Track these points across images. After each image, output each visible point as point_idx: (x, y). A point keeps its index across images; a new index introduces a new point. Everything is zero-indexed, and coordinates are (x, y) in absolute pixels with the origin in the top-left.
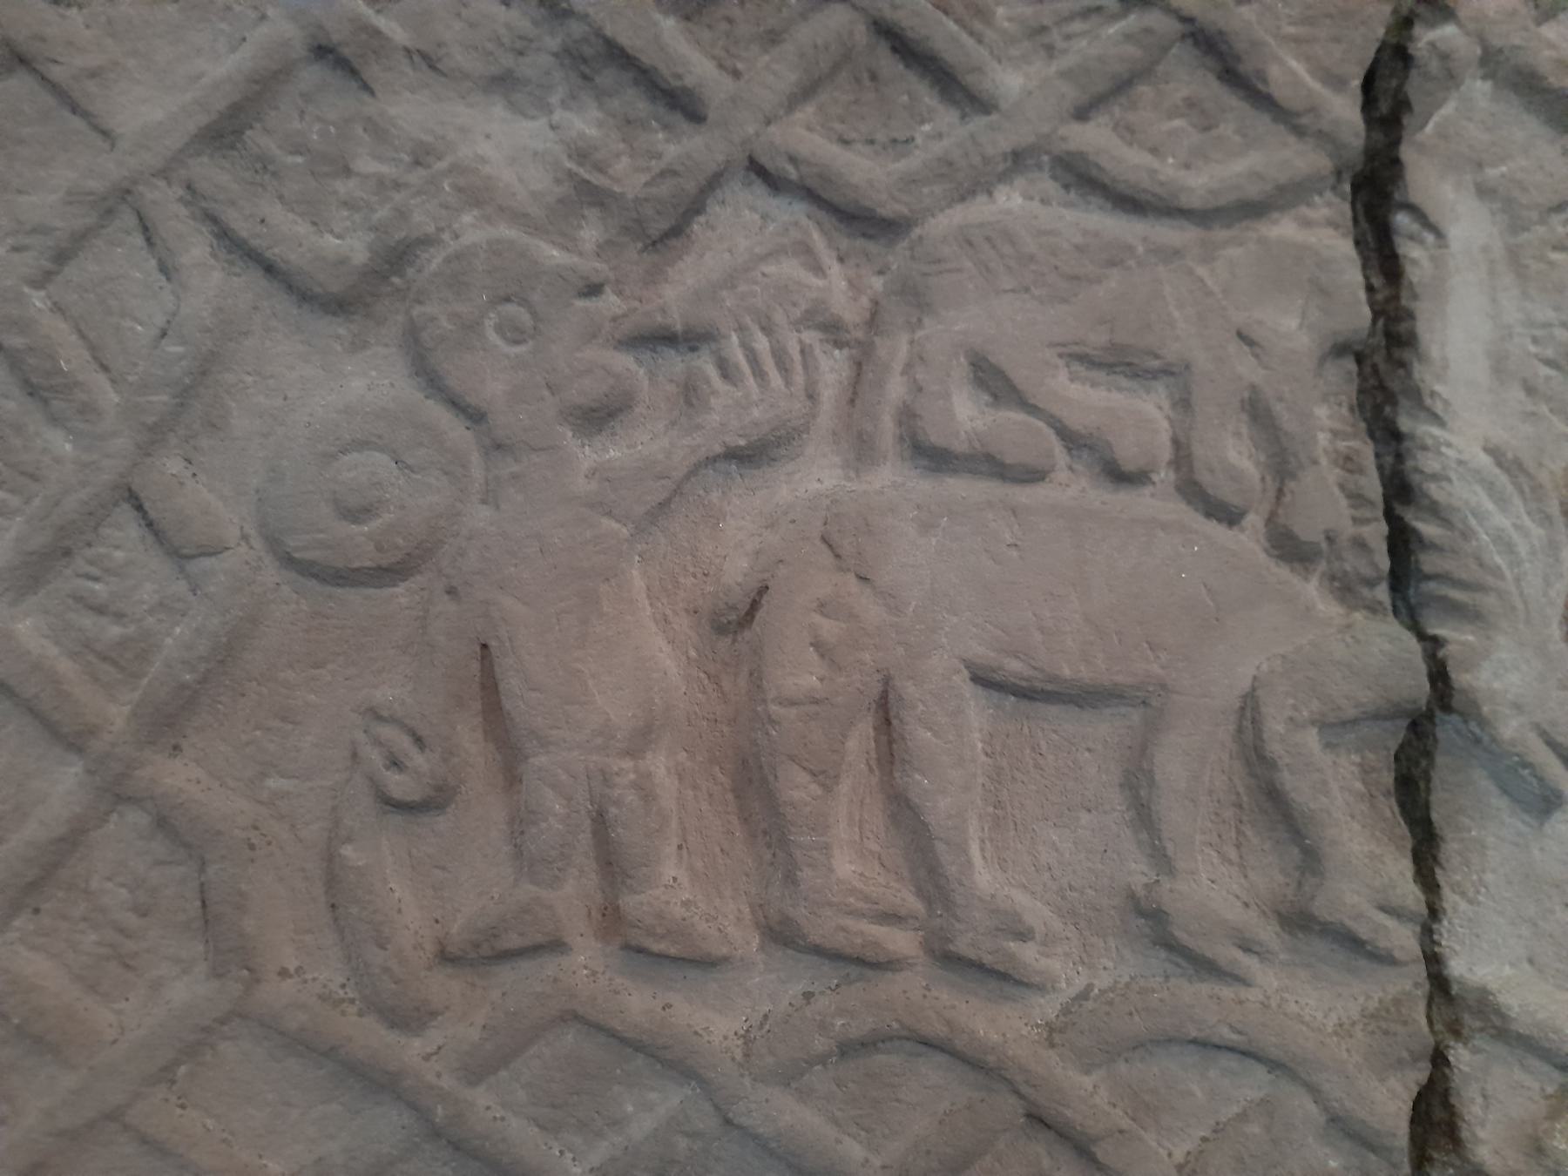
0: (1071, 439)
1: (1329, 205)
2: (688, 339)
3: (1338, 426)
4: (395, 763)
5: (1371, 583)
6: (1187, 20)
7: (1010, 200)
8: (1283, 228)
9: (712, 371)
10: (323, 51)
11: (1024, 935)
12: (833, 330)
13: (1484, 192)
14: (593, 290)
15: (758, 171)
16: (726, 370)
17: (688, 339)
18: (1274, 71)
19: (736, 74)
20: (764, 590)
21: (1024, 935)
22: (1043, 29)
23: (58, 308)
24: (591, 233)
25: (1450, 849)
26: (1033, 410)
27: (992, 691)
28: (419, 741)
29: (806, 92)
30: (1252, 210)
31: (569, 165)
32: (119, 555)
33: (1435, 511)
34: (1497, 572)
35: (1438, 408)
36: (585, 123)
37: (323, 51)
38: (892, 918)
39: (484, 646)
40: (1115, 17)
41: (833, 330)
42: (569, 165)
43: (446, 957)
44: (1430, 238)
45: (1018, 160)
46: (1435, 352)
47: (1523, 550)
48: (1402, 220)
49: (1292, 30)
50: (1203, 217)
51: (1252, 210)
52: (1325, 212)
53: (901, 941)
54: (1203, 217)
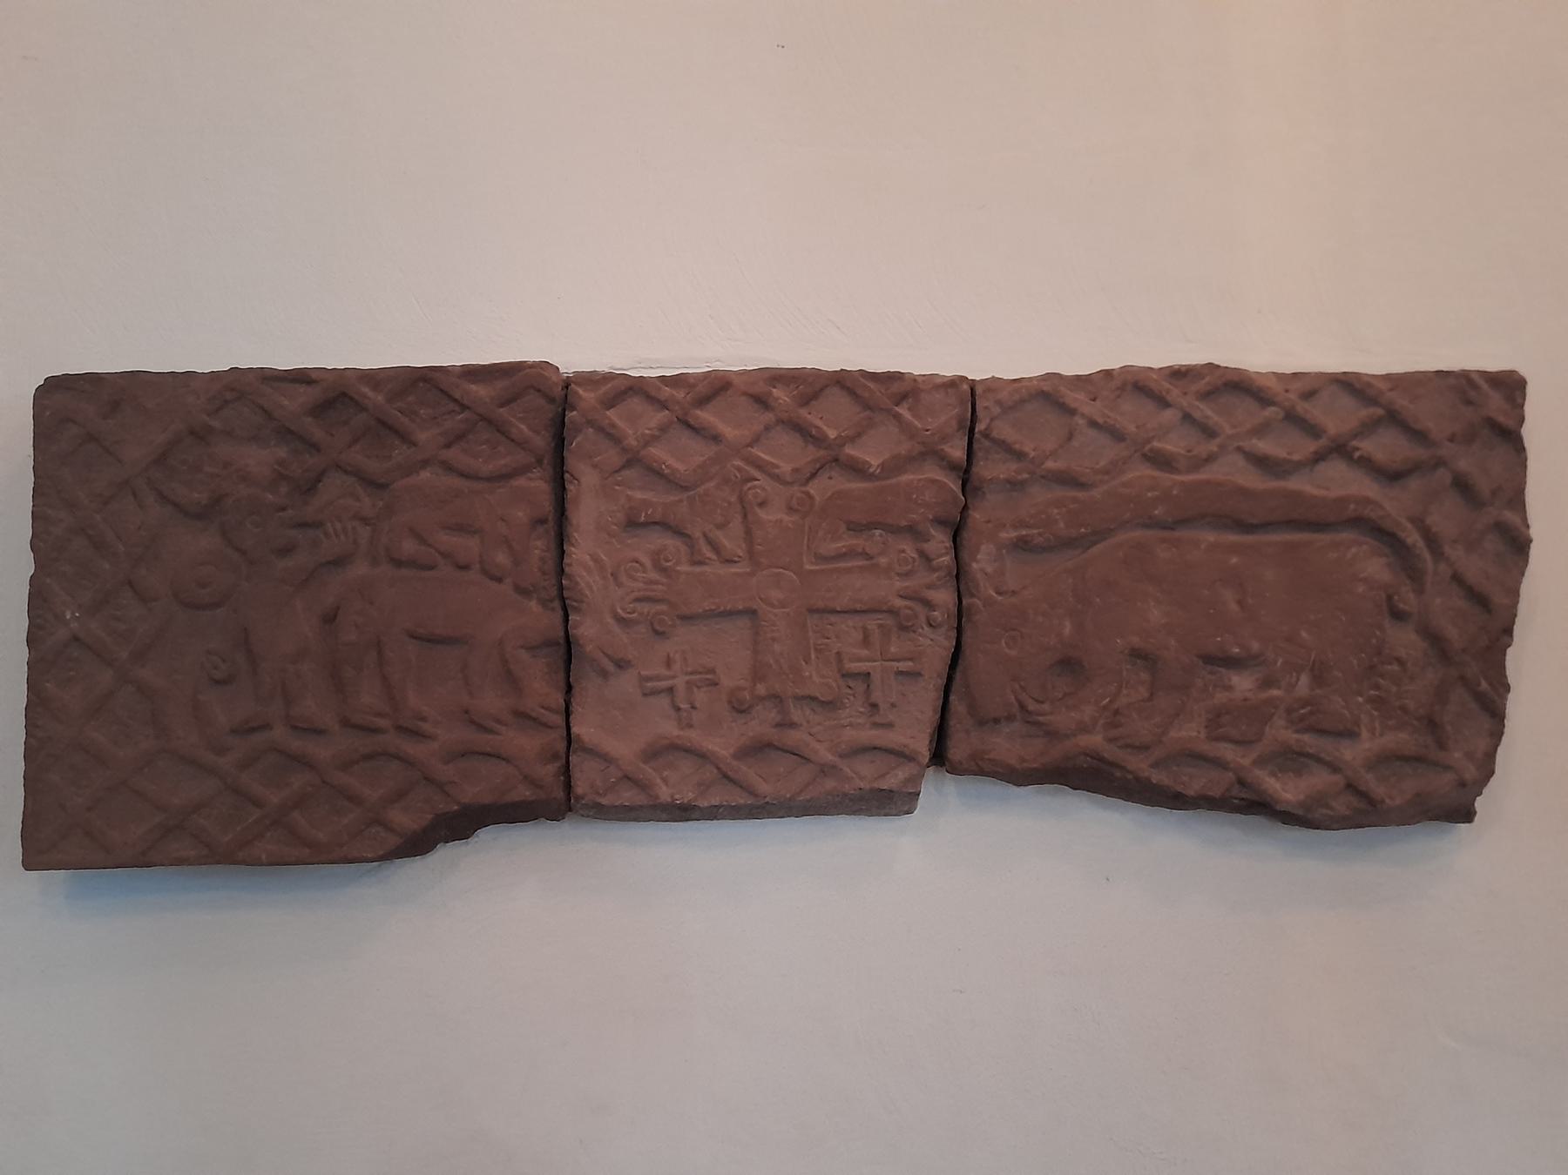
0: (444, 555)
1: (539, 472)
2: (318, 525)
3: (544, 548)
4: (216, 668)
5: (551, 601)
6: (480, 415)
7: (425, 475)
8: (521, 482)
9: (322, 536)
10: (192, 432)
11: (424, 719)
12: (365, 521)
13: (595, 466)
14: (283, 509)
15: (338, 467)
16: (326, 534)
17: (318, 525)
18: (514, 430)
19: (332, 435)
20: (338, 608)
21: (424, 719)
22: (435, 418)
23: (681, 501)
24: (284, 489)
25: (576, 691)
26: (430, 545)
27: (571, 725)
28: (224, 661)
29: (355, 441)
30: (504, 477)
31: (276, 467)
32: (125, 602)
33: (570, 577)
34: (587, 596)
35: (574, 541)
36: (282, 452)
37: (192, 432)
38: (380, 715)
39: (245, 629)
40: (460, 414)
41: (365, 521)
42: (276, 467)
43: (234, 731)
44: (576, 482)
45: (425, 463)
46: (574, 522)
47: (595, 588)
48: (567, 476)
49: (521, 415)
50: (489, 479)
51: (504, 477)
52: (538, 474)
53: (382, 722)
54: (489, 479)
